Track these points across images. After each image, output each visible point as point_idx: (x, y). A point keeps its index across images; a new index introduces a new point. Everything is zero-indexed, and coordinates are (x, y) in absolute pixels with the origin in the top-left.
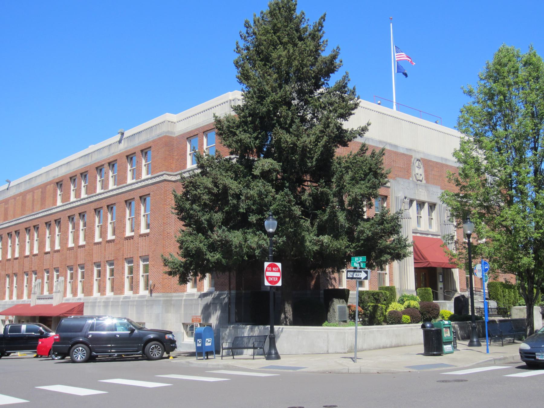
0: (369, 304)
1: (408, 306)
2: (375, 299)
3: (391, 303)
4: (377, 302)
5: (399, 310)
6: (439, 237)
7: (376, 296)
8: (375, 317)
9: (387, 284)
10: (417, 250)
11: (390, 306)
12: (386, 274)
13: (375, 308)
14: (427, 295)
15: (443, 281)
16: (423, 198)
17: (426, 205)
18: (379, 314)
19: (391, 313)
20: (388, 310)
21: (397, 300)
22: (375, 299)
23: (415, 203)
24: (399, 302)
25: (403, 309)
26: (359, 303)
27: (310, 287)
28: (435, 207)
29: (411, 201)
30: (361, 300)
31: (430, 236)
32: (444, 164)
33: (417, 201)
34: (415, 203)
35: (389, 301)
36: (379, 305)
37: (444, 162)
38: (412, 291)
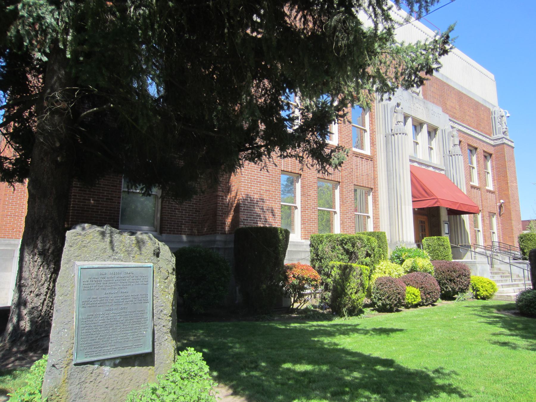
0: (331, 263)
1: (413, 270)
2: (347, 252)
3: (378, 262)
4: (350, 259)
5: (394, 275)
6: (443, 172)
7: (349, 246)
8: (346, 294)
9: (370, 228)
10: (417, 184)
11: (377, 266)
12: (368, 217)
13: (346, 271)
14: (442, 248)
15: (450, 233)
16: (421, 116)
17: (425, 127)
18: (353, 285)
19: (381, 283)
20: (375, 277)
21: (389, 257)
22: (347, 252)
23: (410, 121)
24: (392, 260)
25: (403, 274)
26: (312, 260)
27: (224, 228)
28: (436, 134)
29: (406, 118)
30: (317, 255)
31: (431, 169)
32: (445, 83)
33: (414, 119)
34: (410, 121)
35: (373, 256)
36: (354, 265)
37: (445, 80)
38: (410, 244)
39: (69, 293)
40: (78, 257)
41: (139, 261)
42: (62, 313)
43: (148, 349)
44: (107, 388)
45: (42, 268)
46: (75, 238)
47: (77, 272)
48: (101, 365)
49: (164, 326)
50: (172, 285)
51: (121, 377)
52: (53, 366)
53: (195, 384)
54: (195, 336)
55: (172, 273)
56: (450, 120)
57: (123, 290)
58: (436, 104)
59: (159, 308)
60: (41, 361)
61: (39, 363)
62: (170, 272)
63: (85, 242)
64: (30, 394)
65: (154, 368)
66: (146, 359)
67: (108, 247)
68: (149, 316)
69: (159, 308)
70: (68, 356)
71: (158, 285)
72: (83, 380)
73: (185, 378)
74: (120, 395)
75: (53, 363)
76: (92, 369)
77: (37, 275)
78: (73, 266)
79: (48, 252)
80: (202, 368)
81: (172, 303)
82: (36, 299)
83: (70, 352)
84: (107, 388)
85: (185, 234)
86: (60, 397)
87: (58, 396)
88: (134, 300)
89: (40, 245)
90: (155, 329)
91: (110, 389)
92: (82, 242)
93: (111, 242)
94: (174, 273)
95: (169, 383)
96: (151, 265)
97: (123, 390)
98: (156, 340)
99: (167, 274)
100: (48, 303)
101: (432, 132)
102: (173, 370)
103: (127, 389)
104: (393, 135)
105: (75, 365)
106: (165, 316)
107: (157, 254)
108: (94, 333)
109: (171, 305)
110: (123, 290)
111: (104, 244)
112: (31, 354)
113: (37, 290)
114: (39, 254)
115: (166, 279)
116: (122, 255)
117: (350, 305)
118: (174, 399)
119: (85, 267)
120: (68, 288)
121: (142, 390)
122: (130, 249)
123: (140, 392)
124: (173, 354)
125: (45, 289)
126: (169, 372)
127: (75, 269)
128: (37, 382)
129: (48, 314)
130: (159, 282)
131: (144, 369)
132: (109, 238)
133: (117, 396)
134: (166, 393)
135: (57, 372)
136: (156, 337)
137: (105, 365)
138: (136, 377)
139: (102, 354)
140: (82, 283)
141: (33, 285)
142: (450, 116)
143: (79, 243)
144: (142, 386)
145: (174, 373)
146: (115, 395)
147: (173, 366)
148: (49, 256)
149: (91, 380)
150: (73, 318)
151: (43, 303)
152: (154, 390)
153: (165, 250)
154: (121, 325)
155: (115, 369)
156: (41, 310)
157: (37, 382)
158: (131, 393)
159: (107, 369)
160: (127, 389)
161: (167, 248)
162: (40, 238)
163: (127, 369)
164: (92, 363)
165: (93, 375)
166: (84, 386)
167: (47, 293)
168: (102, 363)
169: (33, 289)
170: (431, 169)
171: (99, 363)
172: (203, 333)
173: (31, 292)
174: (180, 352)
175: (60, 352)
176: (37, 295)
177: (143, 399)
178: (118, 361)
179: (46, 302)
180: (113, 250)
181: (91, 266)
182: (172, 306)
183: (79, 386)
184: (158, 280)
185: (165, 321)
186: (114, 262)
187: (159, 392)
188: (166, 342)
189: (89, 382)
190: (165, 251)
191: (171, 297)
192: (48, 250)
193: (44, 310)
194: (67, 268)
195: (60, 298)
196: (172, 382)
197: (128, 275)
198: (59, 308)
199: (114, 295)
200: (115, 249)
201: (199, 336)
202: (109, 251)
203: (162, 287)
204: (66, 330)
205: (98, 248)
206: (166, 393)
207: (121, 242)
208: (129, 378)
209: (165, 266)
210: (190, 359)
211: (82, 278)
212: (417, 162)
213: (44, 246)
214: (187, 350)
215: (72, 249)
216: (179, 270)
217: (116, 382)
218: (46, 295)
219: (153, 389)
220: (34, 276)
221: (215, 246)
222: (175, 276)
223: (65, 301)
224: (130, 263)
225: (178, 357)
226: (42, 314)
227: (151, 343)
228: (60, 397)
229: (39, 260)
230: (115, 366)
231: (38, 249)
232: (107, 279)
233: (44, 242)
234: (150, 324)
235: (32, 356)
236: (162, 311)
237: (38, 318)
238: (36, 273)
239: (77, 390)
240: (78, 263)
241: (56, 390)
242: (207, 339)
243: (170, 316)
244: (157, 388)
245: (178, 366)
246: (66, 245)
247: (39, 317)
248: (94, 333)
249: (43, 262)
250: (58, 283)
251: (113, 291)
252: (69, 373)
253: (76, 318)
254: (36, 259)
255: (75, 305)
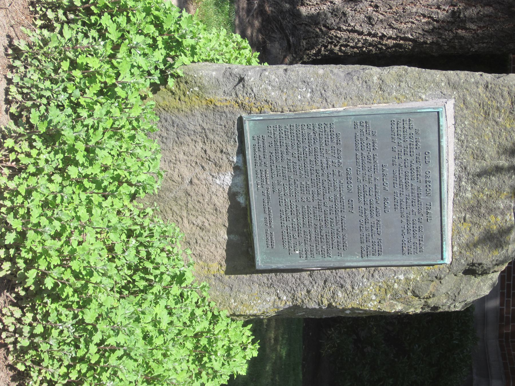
39: (386, 94)
40: (463, 103)
41: (457, 232)
42: (344, 84)
43: (261, 260)
44: (191, 182)
45: (424, 20)
46: (506, 94)
47: (427, 103)
48: (236, 168)
49: (308, 292)
50: (399, 307)
51: (210, 209)
52: (241, 80)
53: (184, 366)
54: (276, 339)
55: (426, 305)
57: (390, 201)
59: (348, 281)
60: (247, 52)
61: (244, 48)
62: (430, 301)
63: (497, 114)
64: (193, 48)
65: (222, 273)
66: (241, 257)
67: (487, 163)
68: (333, 260)
69: (348, 281)
70: (258, 104)
71: (402, 277)
72: (211, 136)
73: (198, 341)
74: (175, 208)
75: (246, 78)
76: (230, 150)
77: (411, 14)
78: (443, 95)
79: (459, 28)
80: (215, 377)
81: (358, 309)
82: (362, 16)
83: (266, 108)
84: (191, 182)
85: (502, 304)
86: (182, 97)
87: (184, 95)
88: (369, 225)
89: (472, 12)
90: (304, 274)
91: (189, 188)
92: (498, 109)
93: (498, 169)
94: (427, 310)
95: (190, 310)
96: (448, 259)
97: (185, 214)
98: (279, 276)
99: (426, 295)
100: (353, 40)
102: (216, 313)
103: (185, 220)
105: (240, 119)
106: (329, 295)
107: (472, 271)
108: (301, 150)
109: (355, 306)
110: (390, 201)
111: (494, 154)
112: (257, 23)
113: (381, 17)
114: (453, 12)
115: (413, 292)
116: (469, 195)
117: (109, 101)
118: (159, 322)
119: (442, 120)
120: (397, 91)
121: (181, 252)
122: (483, 210)
123: (178, 249)
124: (248, 312)
125: (382, 31)
126: (213, 304)
127: (436, 100)
128: (212, 53)
129: (331, 43)
130: (407, 279)
131: (221, 253)
132: (507, 164)
133: (173, 203)
134: (171, 303)
135: (230, 86)
136: (285, 275)
137: (234, 177)
138: (206, 238)
139: (258, 168)
140: (404, 117)
141: (391, 8)
143: (494, 104)
144: (189, 252)
145: (210, 315)
146: (175, 199)
147: (225, 313)
148: (451, 30)
149: (208, 152)
150: (333, 106)
151: (353, 31)
152: (179, 279)
153: (482, 287)
154: (315, 203)
155: (226, 195)
156: (339, 29)
157: (212, 53)
158: (178, 230)
159: (227, 179)
160: (185, 220)
161: (486, 291)
162: (488, 10)
163: (224, 218)
164: (242, 151)
165: (219, 154)
166: (199, 140)
167: (375, 35)
168: (240, 170)
169: (382, 9)
171: (240, 164)
172: (281, 358)
173: (377, 7)
174: (250, 326)
175: (267, 89)
176: (370, 18)
177: (164, 254)
178: (241, 200)
179: (355, 35)
180: (479, 175)
181: (443, 132)
182: (353, 309)
183: (199, 129)
184: (412, 276)
185: (316, 296)
186: (452, 179)
187: (175, 290)
188: (274, 297)
189: (204, 147)
190: (478, 287)
191: (372, 306)
192: (464, 28)
193: (339, 34)
194: (438, 85)
195: (375, 78)
196: (193, 314)
197: (424, 211)
198: (355, 78)
199: (379, 184)
200: (484, 180)
201: (276, 349)
202: (475, 167)
203: (396, 286)
204: (309, 95)
205: (484, 142)
206: (171, 303)
207: (499, 191)
208: (206, 224)
209: (443, 289)
210: (237, 349)
211: (418, 116)
213: (471, 20)
214: (253, 342)
215: (481, 90)
216: (435, 322)
217: (201, 199)
218: (369, 34)
219: (183, 275)
220: (408, 7)
221: (475, 377)
222: (418, 311)
223: (369, 88)
224: (451, 213)
225: (240, 323)
226: (332, 32)
227: (274, 266)
228: (182, 97)
229: (441, 15)
230: (232, 195)
231: (465, 9)
232: (414, 166)
233: (480, 18)
234: (316, 261)
235: (252, 25)
236: (342, 286)
237: (325, 26)
238: (414, 10)
239: (192, 128)
240: (450, 104)
241: (196, 89)
242: (268, 368)
243: (330, 305)
244: (184, 285)
245: (221, 326)
246: (488, 77)
247: (328, 28)
248: (301, 150)
249: (437, 21)
250: (406, 71)
251: (389, 182)
252: (227, 110)
253: (333, 112)
254: (443, 7)
255: (360, 108)
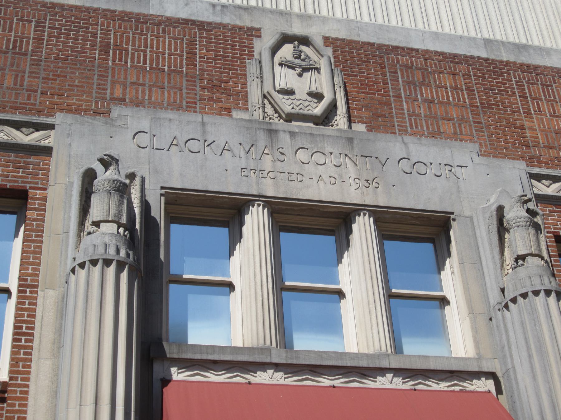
28: (449, 241)
37: (505, 56)
56: (533, 176)
58: (456, 136)
101: (421, 231)
104: (506, 306)
142: (531, 161)
170: (263, 377)
212: (277, 367)
